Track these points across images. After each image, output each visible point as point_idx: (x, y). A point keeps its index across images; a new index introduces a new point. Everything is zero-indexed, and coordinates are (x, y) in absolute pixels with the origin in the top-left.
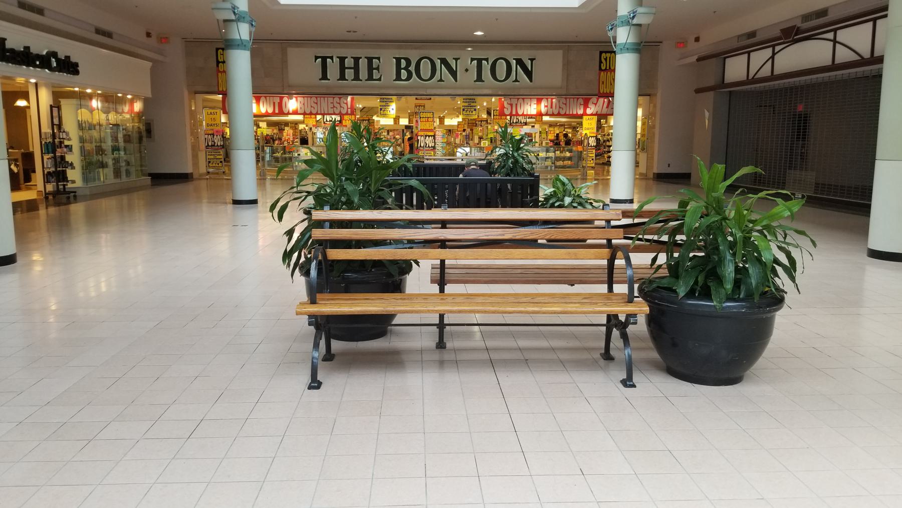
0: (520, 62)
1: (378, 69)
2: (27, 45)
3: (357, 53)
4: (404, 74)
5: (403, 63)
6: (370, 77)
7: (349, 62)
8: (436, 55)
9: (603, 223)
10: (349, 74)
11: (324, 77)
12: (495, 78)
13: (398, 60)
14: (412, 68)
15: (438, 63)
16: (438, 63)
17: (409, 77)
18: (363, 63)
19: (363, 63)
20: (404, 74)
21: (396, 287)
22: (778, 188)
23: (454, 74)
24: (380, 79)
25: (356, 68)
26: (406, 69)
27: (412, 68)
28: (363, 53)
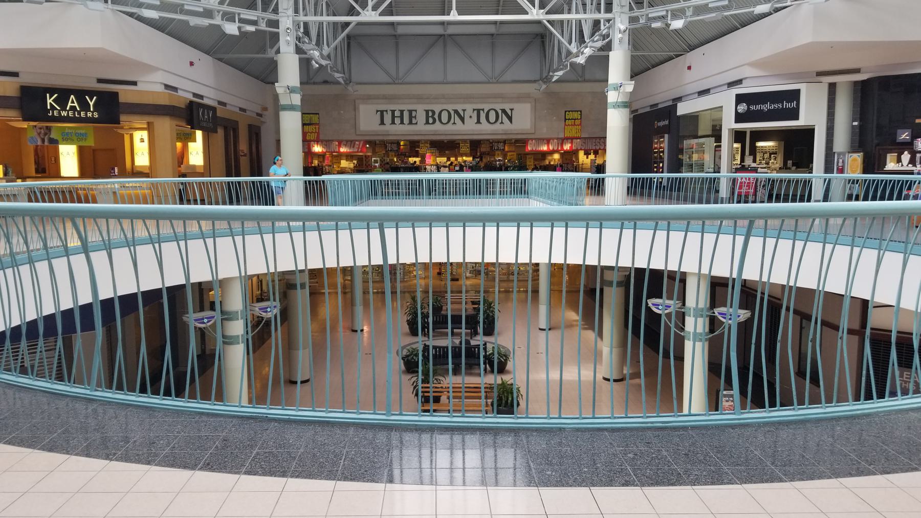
0: (456, 112)
3: (402, 107)
4: (431, 120)
5: (430, 114)
6: (411, 123)
10: (397, 121)
11: (382, 123)
13: (427, 112)
14: (436, 116)
18: (406, 115)
19: (406, 115)
20: (431, 120)
23: (462, 119)
25: (402, 117)
26: (432, 117)
27: (436, 116)
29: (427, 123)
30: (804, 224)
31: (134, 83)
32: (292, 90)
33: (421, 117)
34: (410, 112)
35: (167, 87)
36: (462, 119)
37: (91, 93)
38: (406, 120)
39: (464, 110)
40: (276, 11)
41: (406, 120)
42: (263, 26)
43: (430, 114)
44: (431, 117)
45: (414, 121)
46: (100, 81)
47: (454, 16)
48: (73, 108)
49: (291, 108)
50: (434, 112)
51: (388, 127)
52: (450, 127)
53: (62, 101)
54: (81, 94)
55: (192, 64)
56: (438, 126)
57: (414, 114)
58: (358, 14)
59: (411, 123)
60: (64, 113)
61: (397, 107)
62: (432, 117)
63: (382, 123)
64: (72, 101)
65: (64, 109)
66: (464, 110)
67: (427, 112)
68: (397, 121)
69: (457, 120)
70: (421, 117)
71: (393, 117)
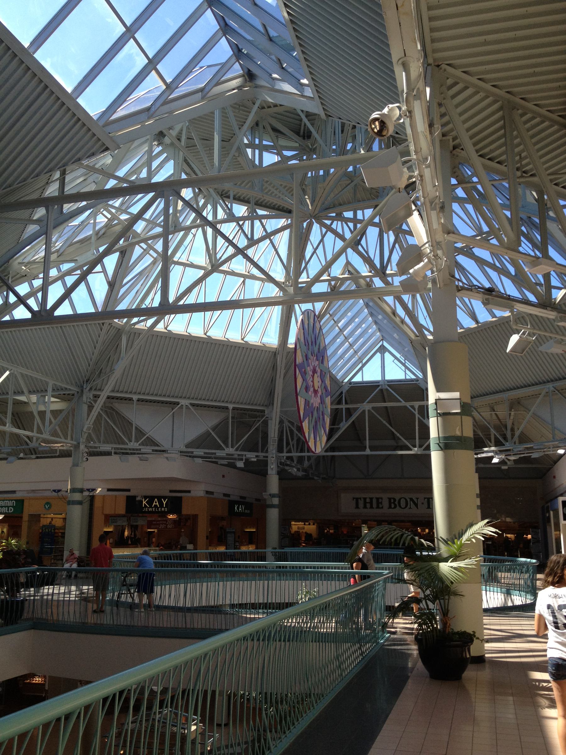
0: (411, 499)
1: (381, 503)
2: (476, 508)
3: (371, 495)
4: (393, 506)
5: (392, 501)
6: (378, 507)
7: (368, 500)
8: (408, 496)
9: (79, 575)
10: (368, 505)
11: (357, 507)
12: (400, 507)
13: (390, 499)
14: (396, 503)
15: (409, 500)
16: (409, 500)
17: (395, 507)
18: (374, 501)
19: (374, 501)
20: (393, 506)
21: (176, 733)
22: (283, 552)
23: (416, 505)
24: (382, 508)
25: (371, 503)
26: (394, 503)
27: (396, 503)
28: (375, 495)
29: (390, 507)
30: (314, 576)
31: (189, 492)
32: (273, 496)
33: (386, 503)
34: (378, 499)
35: (207, 492)
36: (416, 505)
37: (165, 498)
38: (375, 505)
39: (417, 499)
40: (267, 451)
41: (375, 505)
42: (261, 458)
43: (392, 501)
44: (392, 503)
45: (380, 506)
46: (171, 491)
47: (368, 452)
48: (156, 506)
49: (273, 506)
50: (395, 500)
51: (362, 510)
52: (407, 511)
53: (150, 502)
54: (160, 498)
55: (223, 476)
56: (398, 510)
57: (380, 500)
58: (373, 408)
59: (378, 507)
60: (150, 509)
61: (368, 495)
62: (394, 503)
63: (357, 507)
64: (156, 503)
65: (151, 507)
66: (417, 499)
67: (390, 499)
68: (368, 505)
69: (413, 505)
70: (386, 503)
71: (365, 503)
